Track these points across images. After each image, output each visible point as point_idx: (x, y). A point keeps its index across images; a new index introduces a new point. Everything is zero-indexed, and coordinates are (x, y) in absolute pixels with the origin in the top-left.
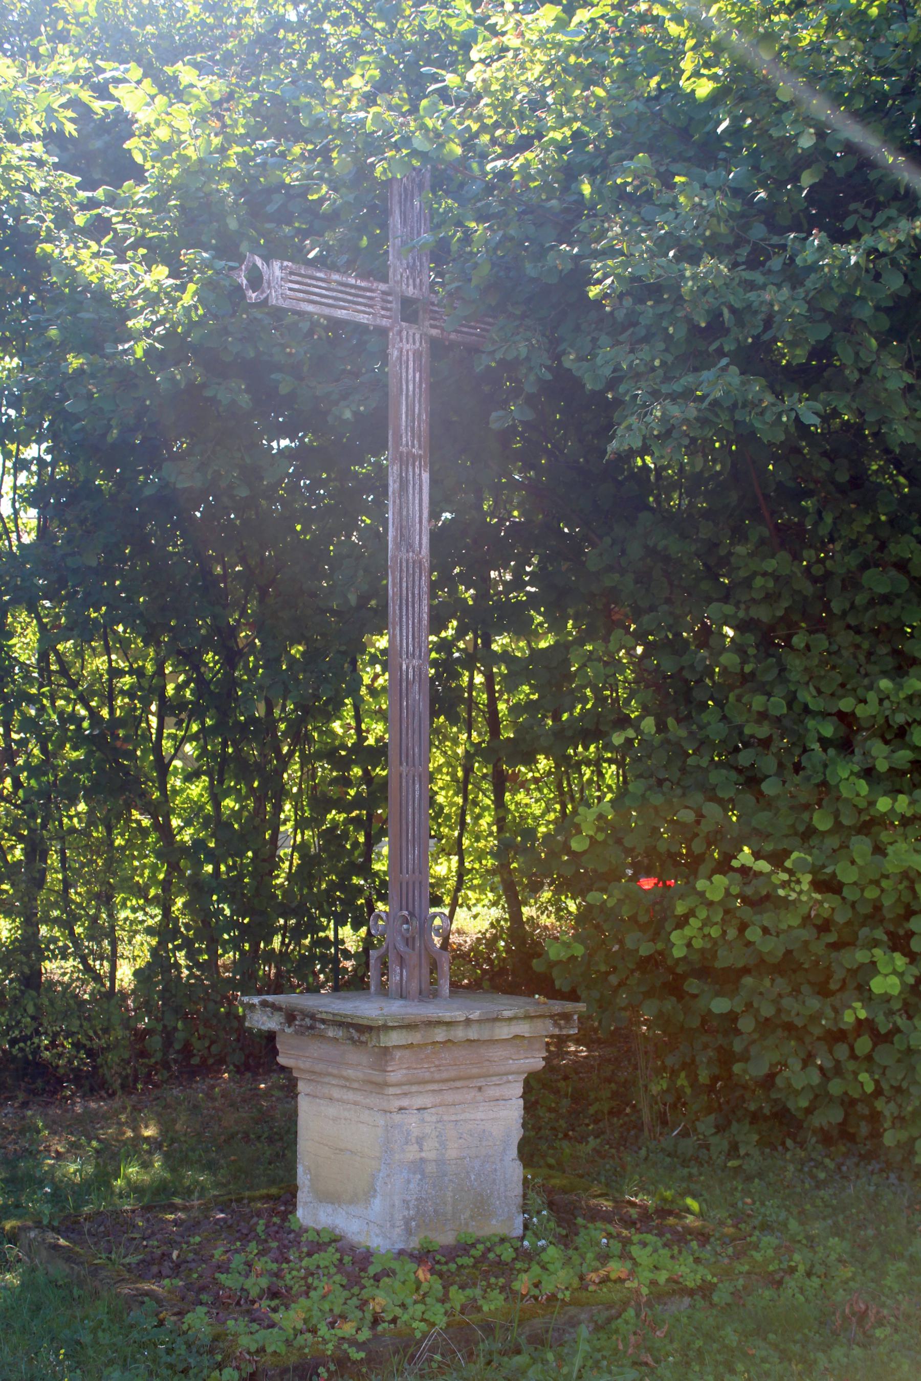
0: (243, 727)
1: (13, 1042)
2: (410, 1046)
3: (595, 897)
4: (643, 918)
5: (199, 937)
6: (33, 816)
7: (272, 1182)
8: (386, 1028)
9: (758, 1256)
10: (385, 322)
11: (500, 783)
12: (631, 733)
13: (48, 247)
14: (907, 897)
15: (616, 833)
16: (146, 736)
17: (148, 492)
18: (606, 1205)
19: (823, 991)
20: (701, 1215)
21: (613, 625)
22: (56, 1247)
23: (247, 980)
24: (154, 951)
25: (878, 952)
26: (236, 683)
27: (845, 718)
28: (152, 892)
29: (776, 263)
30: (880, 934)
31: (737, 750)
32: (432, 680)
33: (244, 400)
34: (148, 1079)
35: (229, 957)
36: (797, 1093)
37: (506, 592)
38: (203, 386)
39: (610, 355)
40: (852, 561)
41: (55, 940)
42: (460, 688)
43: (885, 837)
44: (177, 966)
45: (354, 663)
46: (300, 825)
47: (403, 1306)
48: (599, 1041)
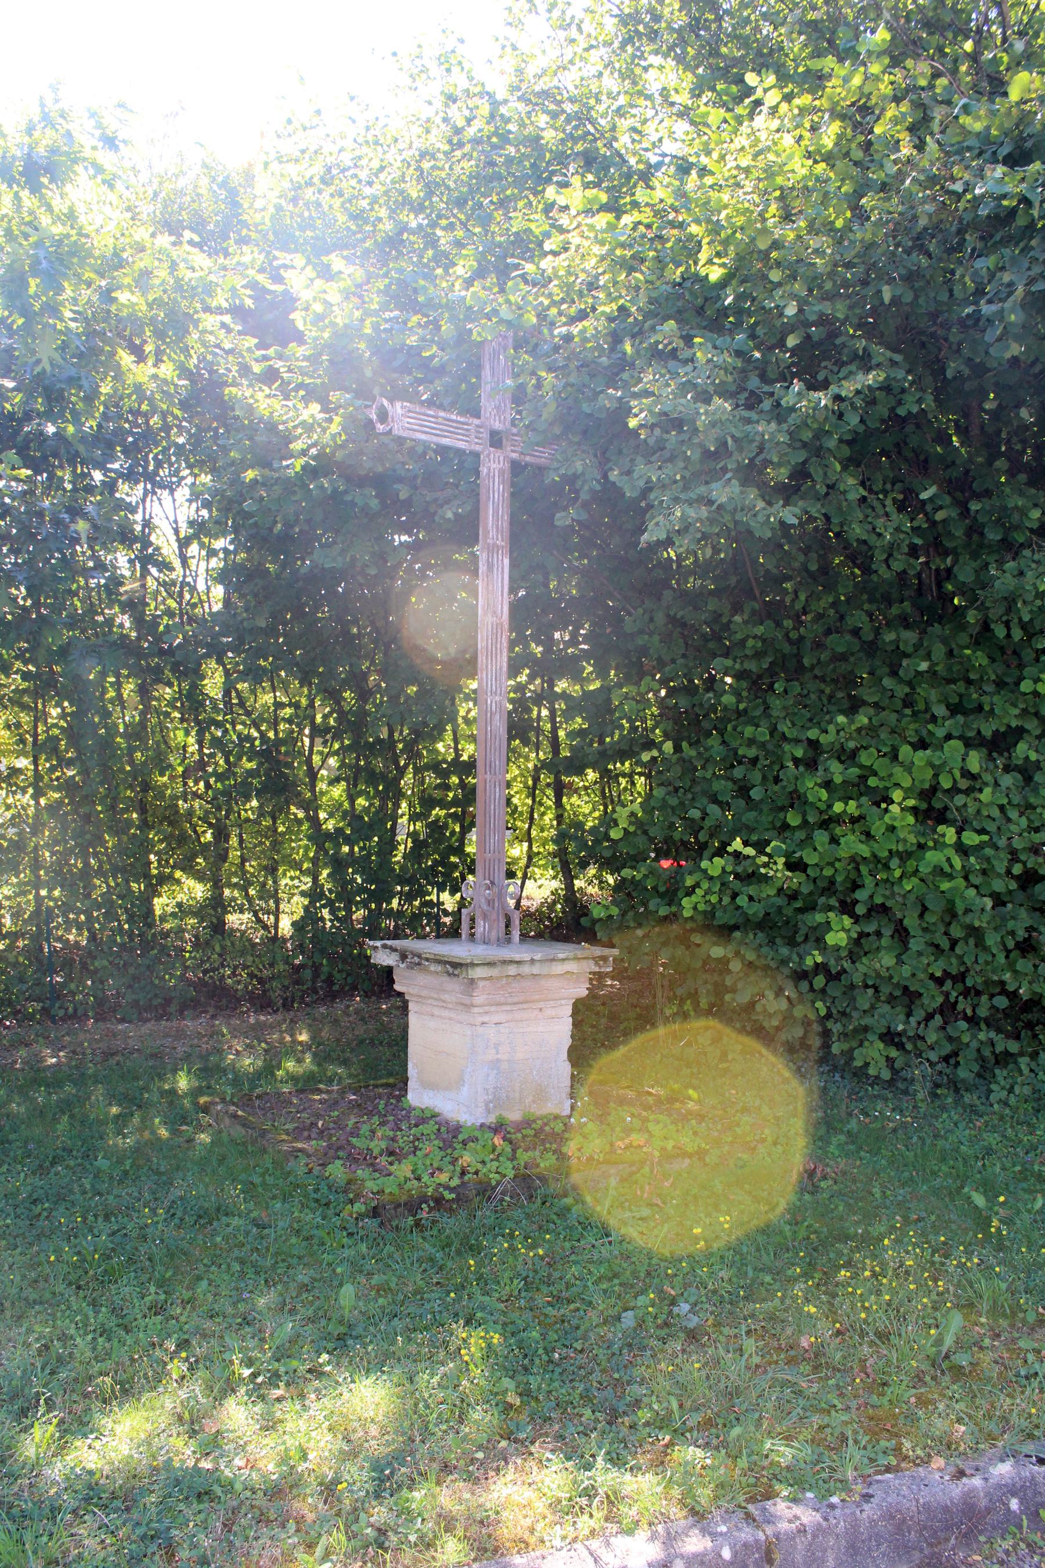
0: (371, 747)
1: (205, 972)
2: (490, 978)
3: (627, 873)
4: (662, 889)
5: (339, 898)
6: (219, 809)
7: (390, 1074)
8: (473, 965)
9: (738, 1131)
10: (478, 448)
11: (560, 790)
12: (655, 753)
13: (234, 390)
14: (853, 875)
15: (641, 825)
16: (301, 753)
17: (303, 571)
18: (631, 1094)
19: (792, 943)
20: (699, 1102)
21: (641, 675)
22: (235, 1116)
23: (373, 931)
24: (306, 909)
25: (831, 914)
26: (367, 713)
27: (814, 744)
28: (305, 866)
29: (767, 405)
30: (833, 902)
31: (733, 766)
32: (510, 713)
33: (374, 504)
34: (302, 1000)
35: (359, 914)
36: (770, 1016)
37: (566, 649)
38: (346, 492)
39: (646, 472)
40: (819, 628)
41: (234, 899)
42: (531, 719)
43: (838, 831)
44: (322, 919)
45: (453, 699)
46: (413, 818)
47: (483, 1162)
48: (629, 978)
